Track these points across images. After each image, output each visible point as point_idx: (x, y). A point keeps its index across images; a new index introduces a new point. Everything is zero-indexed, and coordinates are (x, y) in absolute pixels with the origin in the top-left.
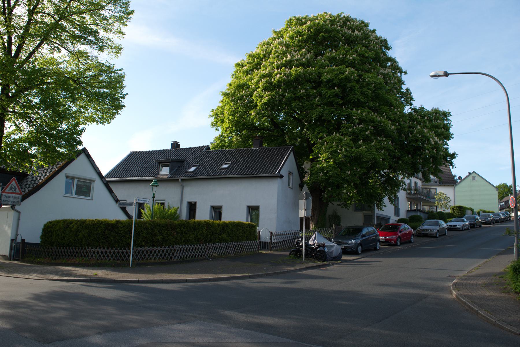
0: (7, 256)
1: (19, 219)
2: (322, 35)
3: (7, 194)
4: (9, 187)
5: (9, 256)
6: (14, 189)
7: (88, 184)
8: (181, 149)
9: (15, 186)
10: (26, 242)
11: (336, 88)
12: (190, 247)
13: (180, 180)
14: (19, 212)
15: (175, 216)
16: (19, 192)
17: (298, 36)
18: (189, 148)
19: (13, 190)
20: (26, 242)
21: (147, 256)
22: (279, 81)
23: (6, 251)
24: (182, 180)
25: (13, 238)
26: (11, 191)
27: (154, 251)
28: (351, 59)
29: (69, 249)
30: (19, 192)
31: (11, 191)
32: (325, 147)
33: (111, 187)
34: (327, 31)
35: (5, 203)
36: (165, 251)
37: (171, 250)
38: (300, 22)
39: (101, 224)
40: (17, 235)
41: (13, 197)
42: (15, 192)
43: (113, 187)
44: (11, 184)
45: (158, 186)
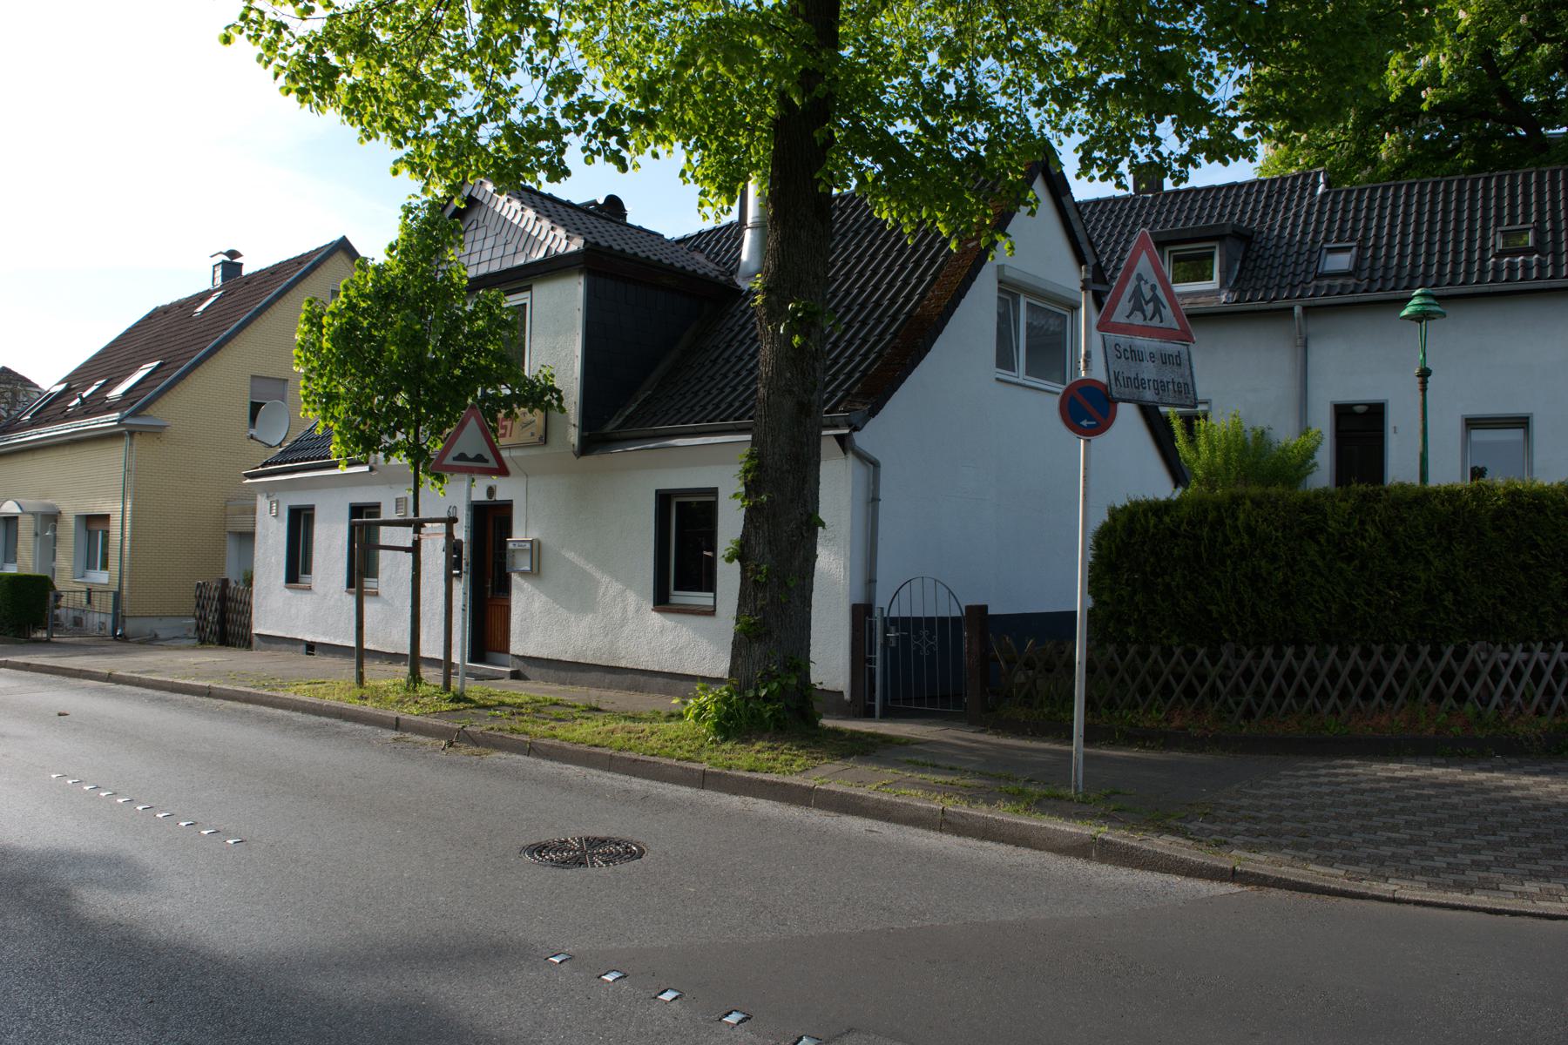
0: (842, 693)
1: (874, 500)
3: (1122, 339)
4: (1129, 289)
5: (852, 694)
6: (1151, 304)
7: (1053, 324)
8: (246, 276)
9: (1153, 288)
12: (1524, 656)
13: (1297, 310)
14: (875, 464)
18: (260, 271)
19: (1150, 308)
20: (991, 612)
24: (1305, 309)
25: (859, 600)
26: (1138, 319)
27: (1511, 668)
31: (1138, 319)
40: (871, 582)
41: (1152, 355)
42: (1156, 322)
44: (1134, 276)
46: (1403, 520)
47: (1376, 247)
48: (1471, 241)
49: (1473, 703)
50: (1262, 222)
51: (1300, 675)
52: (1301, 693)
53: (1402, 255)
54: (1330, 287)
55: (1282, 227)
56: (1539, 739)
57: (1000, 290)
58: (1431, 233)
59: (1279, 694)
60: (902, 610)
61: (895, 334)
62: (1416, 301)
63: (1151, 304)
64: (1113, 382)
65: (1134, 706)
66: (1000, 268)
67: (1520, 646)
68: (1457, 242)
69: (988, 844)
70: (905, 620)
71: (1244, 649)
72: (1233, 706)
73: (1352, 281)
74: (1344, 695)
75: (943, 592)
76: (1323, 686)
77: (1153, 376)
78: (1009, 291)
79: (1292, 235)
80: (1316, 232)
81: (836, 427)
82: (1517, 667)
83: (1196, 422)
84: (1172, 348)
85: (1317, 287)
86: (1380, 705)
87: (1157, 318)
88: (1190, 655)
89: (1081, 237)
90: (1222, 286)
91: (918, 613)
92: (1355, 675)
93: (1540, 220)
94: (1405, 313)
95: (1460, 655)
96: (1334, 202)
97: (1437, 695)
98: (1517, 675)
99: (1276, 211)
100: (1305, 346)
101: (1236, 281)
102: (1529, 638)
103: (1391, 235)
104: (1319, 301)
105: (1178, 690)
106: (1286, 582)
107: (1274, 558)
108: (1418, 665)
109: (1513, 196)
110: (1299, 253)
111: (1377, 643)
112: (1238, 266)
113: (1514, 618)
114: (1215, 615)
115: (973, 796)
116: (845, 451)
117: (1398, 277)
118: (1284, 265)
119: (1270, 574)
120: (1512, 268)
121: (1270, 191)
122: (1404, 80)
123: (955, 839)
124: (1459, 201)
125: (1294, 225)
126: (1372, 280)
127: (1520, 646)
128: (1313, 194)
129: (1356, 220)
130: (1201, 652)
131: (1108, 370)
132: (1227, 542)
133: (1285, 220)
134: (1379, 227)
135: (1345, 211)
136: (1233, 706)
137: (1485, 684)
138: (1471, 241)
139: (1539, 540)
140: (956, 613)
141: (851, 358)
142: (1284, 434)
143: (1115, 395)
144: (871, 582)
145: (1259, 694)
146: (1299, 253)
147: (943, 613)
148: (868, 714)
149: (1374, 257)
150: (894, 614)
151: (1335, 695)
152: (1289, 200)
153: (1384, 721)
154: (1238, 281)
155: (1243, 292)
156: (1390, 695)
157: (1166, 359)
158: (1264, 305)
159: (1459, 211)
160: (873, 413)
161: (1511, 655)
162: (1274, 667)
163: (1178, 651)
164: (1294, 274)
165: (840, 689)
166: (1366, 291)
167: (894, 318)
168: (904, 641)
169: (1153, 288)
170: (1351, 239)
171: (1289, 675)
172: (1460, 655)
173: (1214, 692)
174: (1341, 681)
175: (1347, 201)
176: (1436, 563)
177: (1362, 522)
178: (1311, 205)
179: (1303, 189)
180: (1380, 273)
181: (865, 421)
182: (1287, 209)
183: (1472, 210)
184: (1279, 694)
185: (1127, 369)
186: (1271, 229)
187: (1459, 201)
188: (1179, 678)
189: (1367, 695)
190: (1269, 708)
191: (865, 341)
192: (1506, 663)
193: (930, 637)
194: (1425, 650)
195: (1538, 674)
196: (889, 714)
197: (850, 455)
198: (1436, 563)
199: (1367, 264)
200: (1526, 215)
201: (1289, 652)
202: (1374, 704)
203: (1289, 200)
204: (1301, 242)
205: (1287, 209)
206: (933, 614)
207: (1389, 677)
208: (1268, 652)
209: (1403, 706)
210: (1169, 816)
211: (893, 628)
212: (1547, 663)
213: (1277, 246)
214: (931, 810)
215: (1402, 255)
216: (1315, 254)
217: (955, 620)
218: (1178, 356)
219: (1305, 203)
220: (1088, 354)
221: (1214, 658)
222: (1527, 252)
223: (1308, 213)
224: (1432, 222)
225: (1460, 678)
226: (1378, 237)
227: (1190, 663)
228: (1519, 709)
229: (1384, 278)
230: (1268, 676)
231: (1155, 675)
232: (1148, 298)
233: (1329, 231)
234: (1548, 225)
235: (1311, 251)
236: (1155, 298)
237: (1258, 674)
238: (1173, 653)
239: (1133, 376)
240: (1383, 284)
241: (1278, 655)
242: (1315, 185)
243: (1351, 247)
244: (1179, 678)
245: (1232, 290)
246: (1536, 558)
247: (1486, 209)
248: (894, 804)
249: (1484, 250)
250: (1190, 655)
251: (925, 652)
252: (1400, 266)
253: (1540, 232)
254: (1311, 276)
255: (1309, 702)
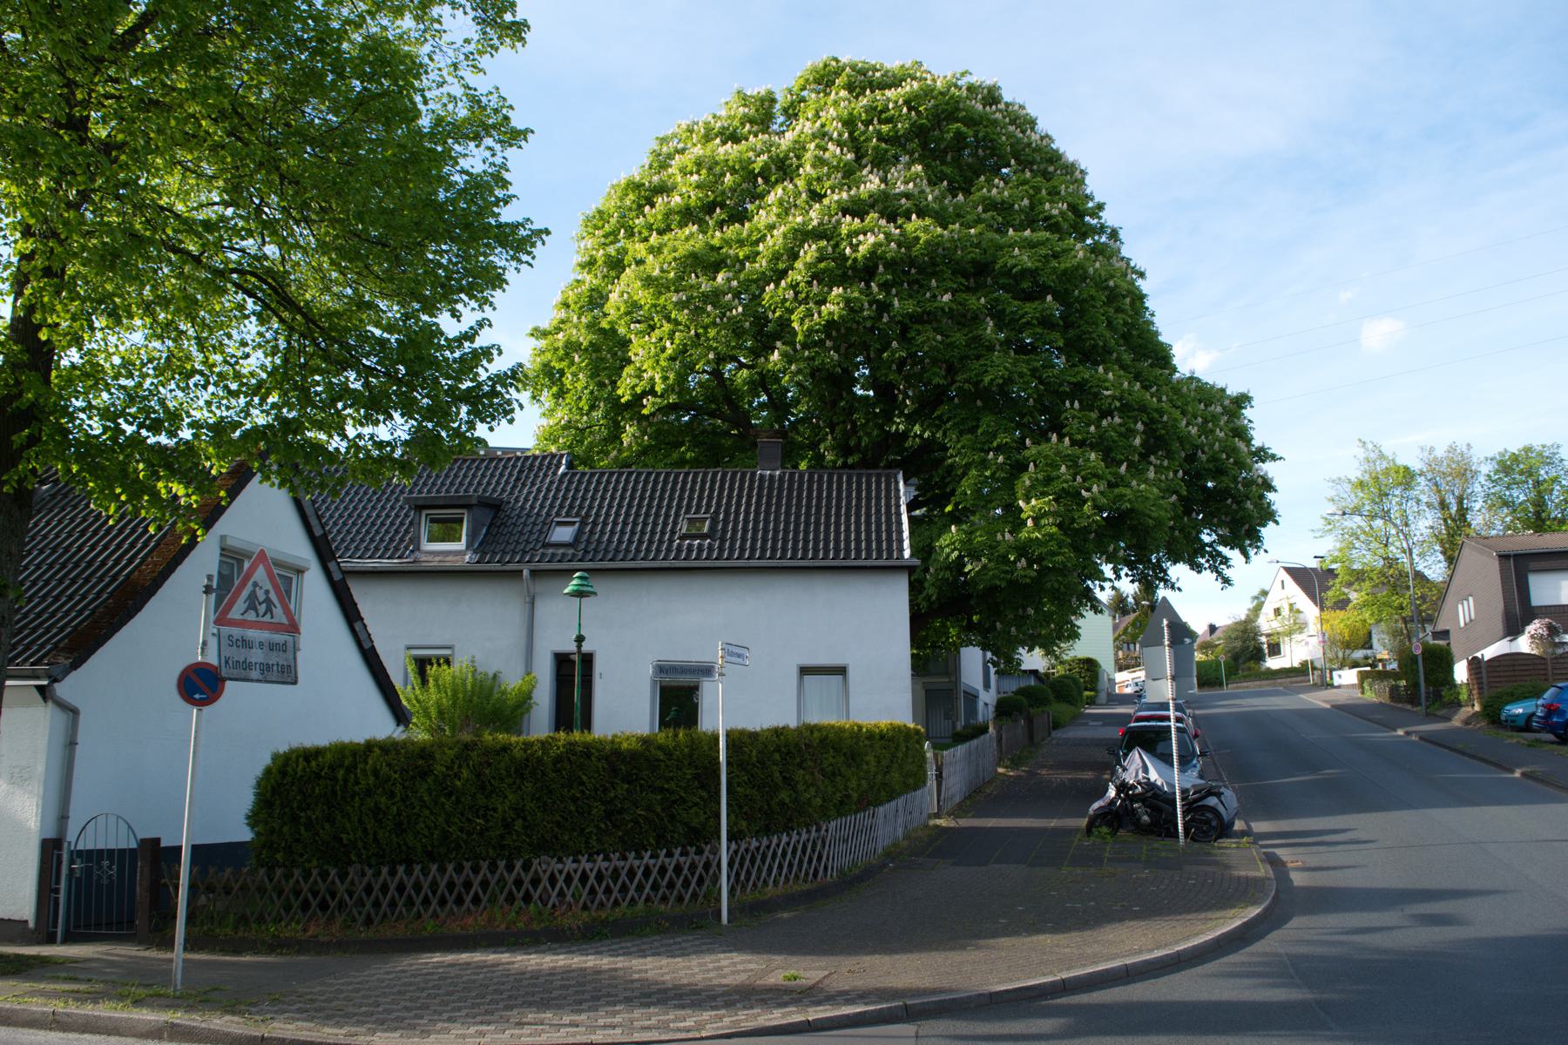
0: (26, 922)
1: (71, 744)
2: (957, 128)
3: (236, 632)
4: (245, 593)
6: (264, 605)
9: (267, 592)
10: (163, 844)
11: (1049, 298)
13: (526, 573)
14: (74, 712)
15: (510, 713)
16: (285, 620)
17: (875, 122)
19: (262, 609)
20: (163, 844)
21: (600, 891)
22: (873, 255)
23: (20, 901)
24: (534, 573)
25: (51, 834)
26: (251, 616)
27: (564, 875)
28: (1055, 216)
29: (426, 875)
30: (285, 620)
31: (251, 616)
32: (1030, 478)
33: (355, 598)
34: (972, 121)
35: (235, 673)
36: (624, 873)
37: (678, 869)
38: (863, 80)
39: (588, 755)
40: (63, 818)
41: (261, 644)
42: (267, 618)
43: (359, 592)
45: (595, 594)
46: (490, 765)
47: (595, 523)
48: (665, 524)
49: (536, 903)
50: (511, 493)
51: (409, 889)
52: (410, 903)
53: (612, 532)
54: (553, 555)
55: (526, 500)
56: (579, 927)
57: (221, 555)
58: (637, 515)
59: (393, 904)
60: (87, 844)
61: (111, 594)
62: (575, 582)
63: (264, 605)
64: (223, 664)
65: (277, 920)
66: (223, 538)
67: (571, 858)
68: (655, 524)
69: (86, 1036)
70: (90, 852)
71: (366, 868)
72: (356, 914)
73: (571, 551)
74: (443, 902)
75: (123, 827)
76: (426, 895)
77: (259, 661)
78: (232, 557)
79: (532, 507)
80: (551, 506)
81: (38, 678)
82: (568, 873)
83: (429, 667)
84: (279, 638)
85: (543, 555)
86: (469, 909)
87: (269, 615)
88: (324, 875)
89: (309, 511)
90: (467, 548)
91: (101, 846)
92: (451, 885)
93: (717, 512)
94: (566, 591)
95: (527, 867)
96: (570, 482)
97: (510, 899)
98: (568, 880)
99: (524, 485)
100: (533, 603)
101: (480, 544)
102: (580, 852)
103: (608, 515)
104: (544, 566)
105: (314, 904)
106: (399, 814)
107: (392, 795)
108: (497, 876)
109: (702, 490)
110: (534, 524)
111: (467, 860)
112: (484, 531)
113: (566, 838)
114: (345, 842)
115: (80, 997)
116: (45, 699)
117: (606, 551)
118: (521, 533)
119: (388, 808)
120: (690, 547)
121: (522, 466)
122: (633, 388)
123: (61, 1035)
124: (663, 490)
125: (536, 499)
126: (586, 552)
127: (571, 858)
128: (555, 474)
129: (584, 499)
130: (333, 872)
131: (220, 655)
132: (357, 783)
133: (529, 493)
134: (600, 507)
135: (577, 490)
136: (356, 914)
137: (545, 888)
138: (665, 524)
139: (584, 778)
140: (133, 845)
141: (67, 613)
142: (512, 681)
143: (224, 674)
144: (63, 818)
145: (377, 904)
146: (534, 524)
147: (123, 846)
148: (50, 940)
149: (592, 532)
150: (80, 847)
151: (435, 902)
152: (536, 476)
153: (470, 921)
154: (483, 545)
155: (484, 553)
156: (476, 900)
157: (273, 647)
158: (498, 567)
159: (661, 498)
160: (75, 666)
161: (565, 864)
162: (389, 881)
163: (315, 872)
164: (528, 542)
165: (25, 918)
166: (580, 560)
167: (114, 578)
168: (88, 872)
169: (267, 592)
170: (577, 515)
171: (401, 888)
172: (527, 867)
173: (342, 905)
174: (439, 892)
175: (580, 482)
176: (511, 797)
177: (460, 767)
178: (552, 482)
179: (549, 468)
180: (593, 546)
181: (66, 673)
182: (533, 484)
183: (671, 499)
184: (393, 904)
185: (239, 655)
186: (517, 500)
187: (663, 490)
188: (315, 894)
189: (459, 901)
190: (385, 915)
191: (84, 597)
192: (561, 872)
193: (110, 867)
194: (502, 864)
195: (584, 878)
196: (69, 939)
197: (50, 704)
198: (511, 797)
199: (585, 537)
200: (709, 506)
201: (401, 869)
202: (464, 908)
203: (536, 476)
204: (538, 514)
205: (533, 484)
206: (114, 847)
207: (476, 887)
208: (385, 870)
209: (485, 908)
210: (240, 1003)
211: (79, 860)
212: (591, 870)
213: (519, 516)
214: (45, 1013)
215: (612, 532)
216: (548, 525)
217: (132, 850)
218: (285, 644)
219: (548, 481)
220: (205, 643)
221: (343, 876)
222: (703, 537)
223: (548, 490)
224: (640, 506)
225: (527, 885)
226: (598, 515)
227: (324, 881)
228: (570, 905)
229: (596, 551)
230: (385, 889)
231: (297, 893)
232: (261, 600)
233: (561, 506)
234: (721, 516)
235: (544, 523)
236: (268, 601)
237: (377, 887)
238: (463, 868)
239: (242, 660)
240: (604, 555)
241: (393, 873)
242: (558, 467)
243: (574, 523)
244: (315, 894)
245: (475, 552)
246: (583, 792)
247: (681, 498)
248: (13, 1011)
249: (673, 532)
250: (324, 875)
251: (105, 881)
252: (610, 541)
253: (714, 521)
254: (540, 545)
255: (415, 909)
